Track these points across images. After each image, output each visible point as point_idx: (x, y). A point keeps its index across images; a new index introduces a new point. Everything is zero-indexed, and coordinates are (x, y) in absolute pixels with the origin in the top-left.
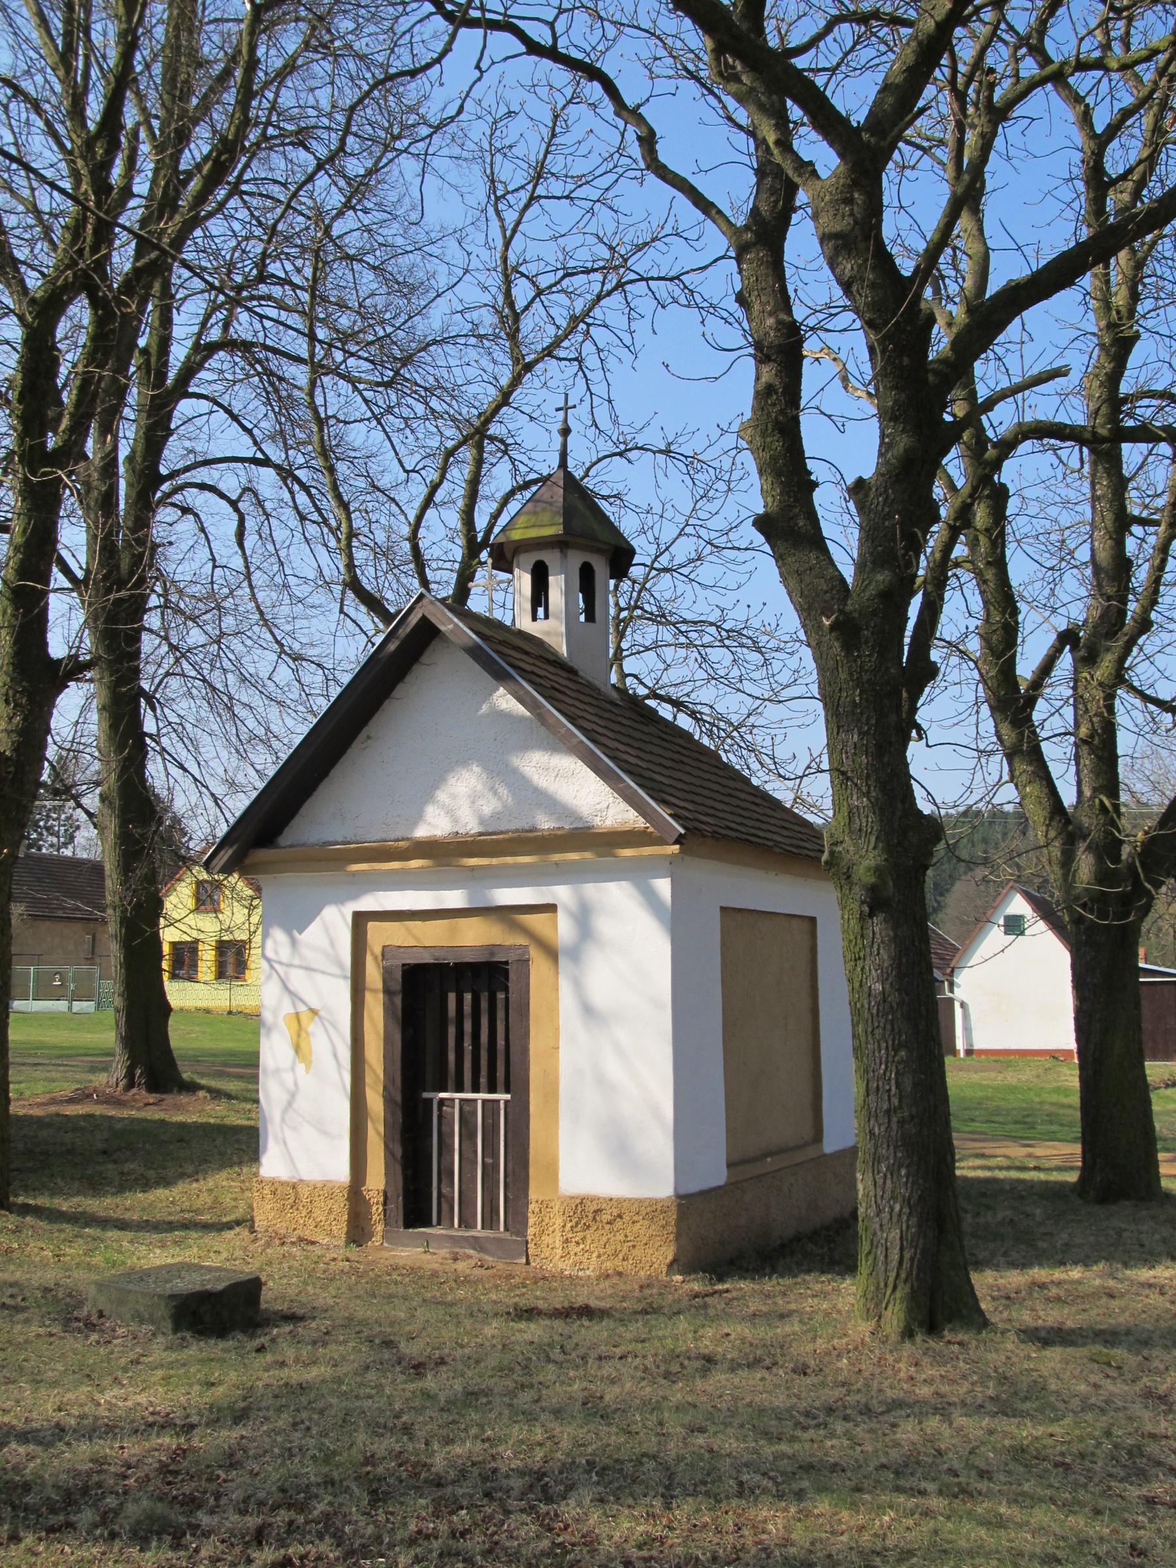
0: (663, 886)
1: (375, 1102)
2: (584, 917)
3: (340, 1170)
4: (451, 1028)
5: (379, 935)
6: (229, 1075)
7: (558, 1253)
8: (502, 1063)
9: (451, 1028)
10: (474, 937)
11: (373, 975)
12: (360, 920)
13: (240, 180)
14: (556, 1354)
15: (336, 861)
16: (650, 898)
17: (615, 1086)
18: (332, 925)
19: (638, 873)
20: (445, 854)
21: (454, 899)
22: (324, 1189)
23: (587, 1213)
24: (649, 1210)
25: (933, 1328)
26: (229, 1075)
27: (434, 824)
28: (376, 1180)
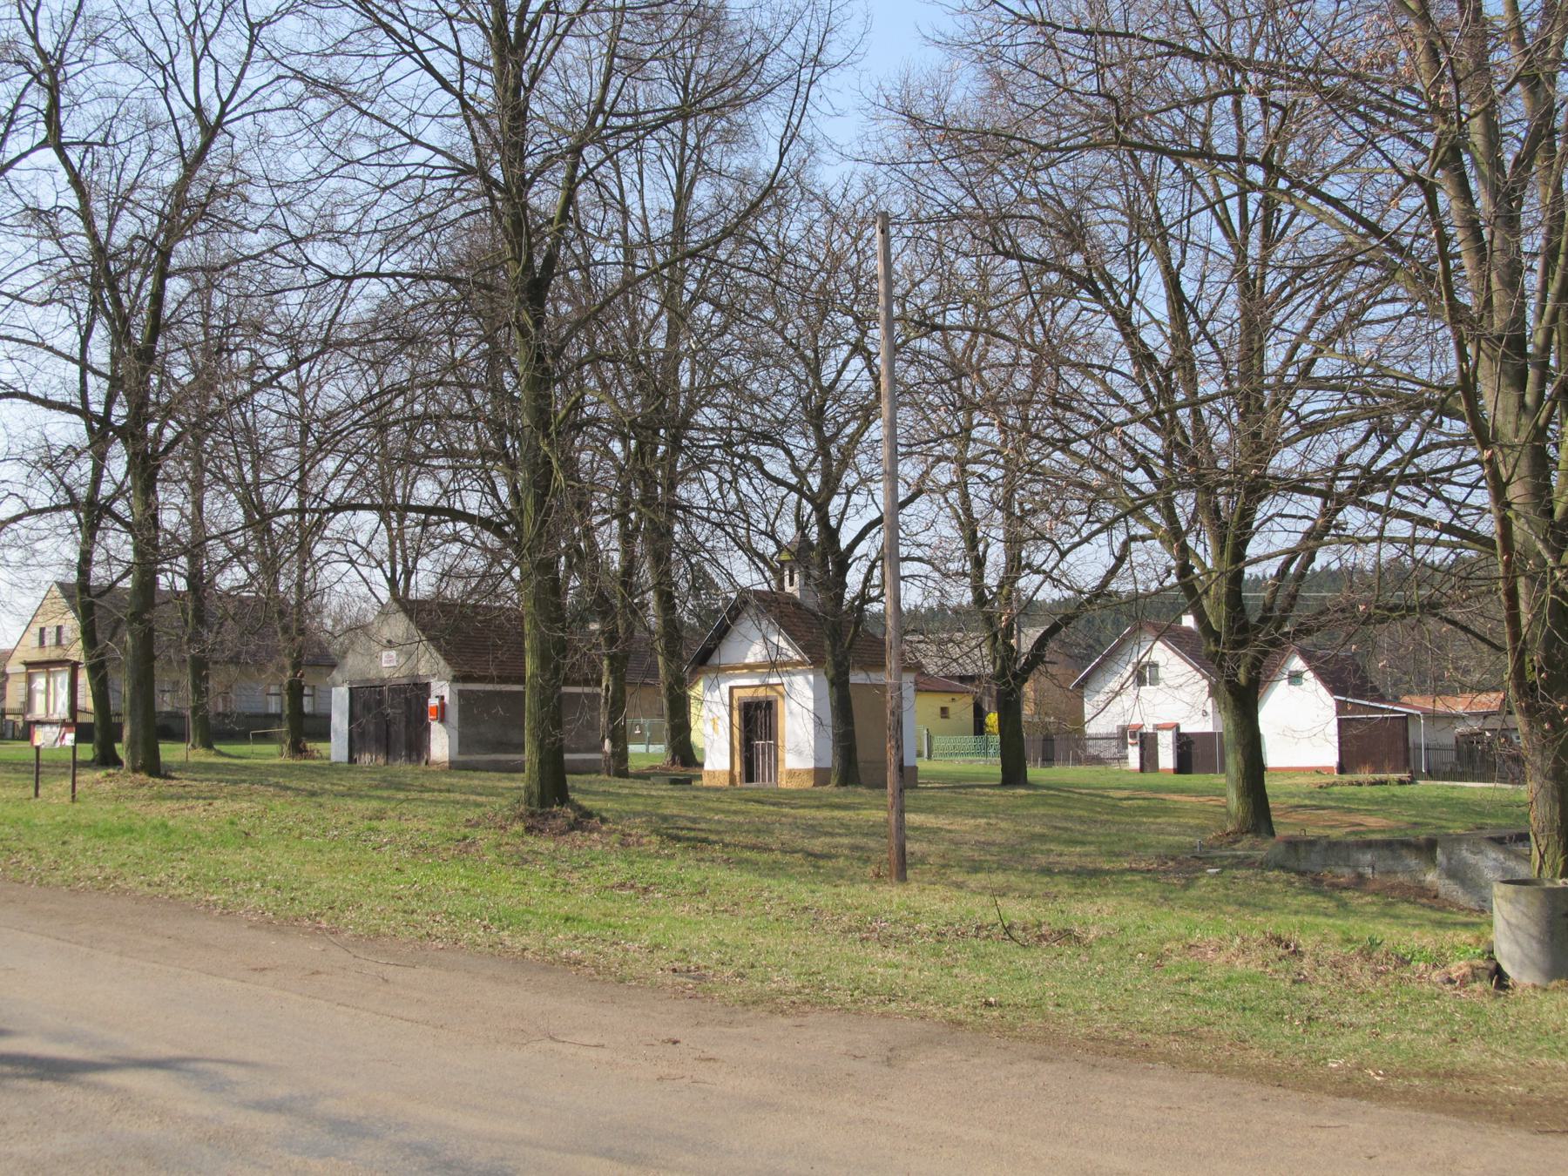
0: (811, 677)
1: (737, 744)
2: (790, 684)
3: (727, 767)
4: (756, 721)
5: (737, 693)
6: (596, 793)
7: (784, 783)
8: (771, 732)
9: (756, 721)
10: (761, 693)
11: (735, 704)
12: (731, 688)
13: (673, 629)
14: (1017, 933)
15: (720, 670)
16: (808, 682)
17: (800, 737)
18: (725, 687)
19: (803, 673)
20: (751, 668)
21: (756, 682)
22: (722, 772)
23: (792, 774)
24: (808, 771)
25: (844, 784)
26: (596, 793)
27: (750, 659)
28: (737, 769)
